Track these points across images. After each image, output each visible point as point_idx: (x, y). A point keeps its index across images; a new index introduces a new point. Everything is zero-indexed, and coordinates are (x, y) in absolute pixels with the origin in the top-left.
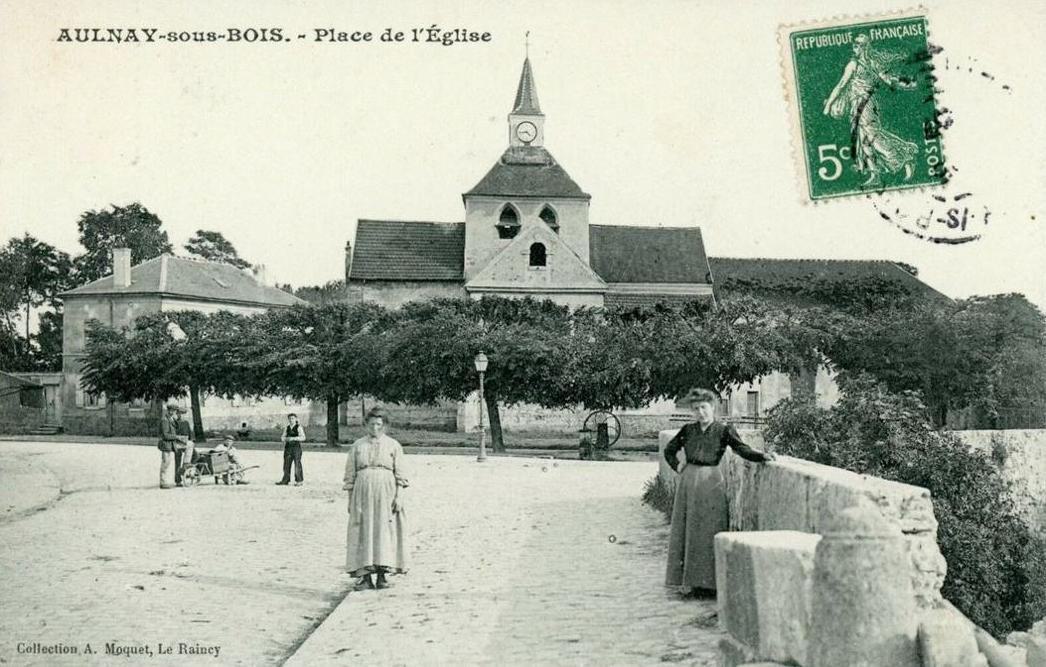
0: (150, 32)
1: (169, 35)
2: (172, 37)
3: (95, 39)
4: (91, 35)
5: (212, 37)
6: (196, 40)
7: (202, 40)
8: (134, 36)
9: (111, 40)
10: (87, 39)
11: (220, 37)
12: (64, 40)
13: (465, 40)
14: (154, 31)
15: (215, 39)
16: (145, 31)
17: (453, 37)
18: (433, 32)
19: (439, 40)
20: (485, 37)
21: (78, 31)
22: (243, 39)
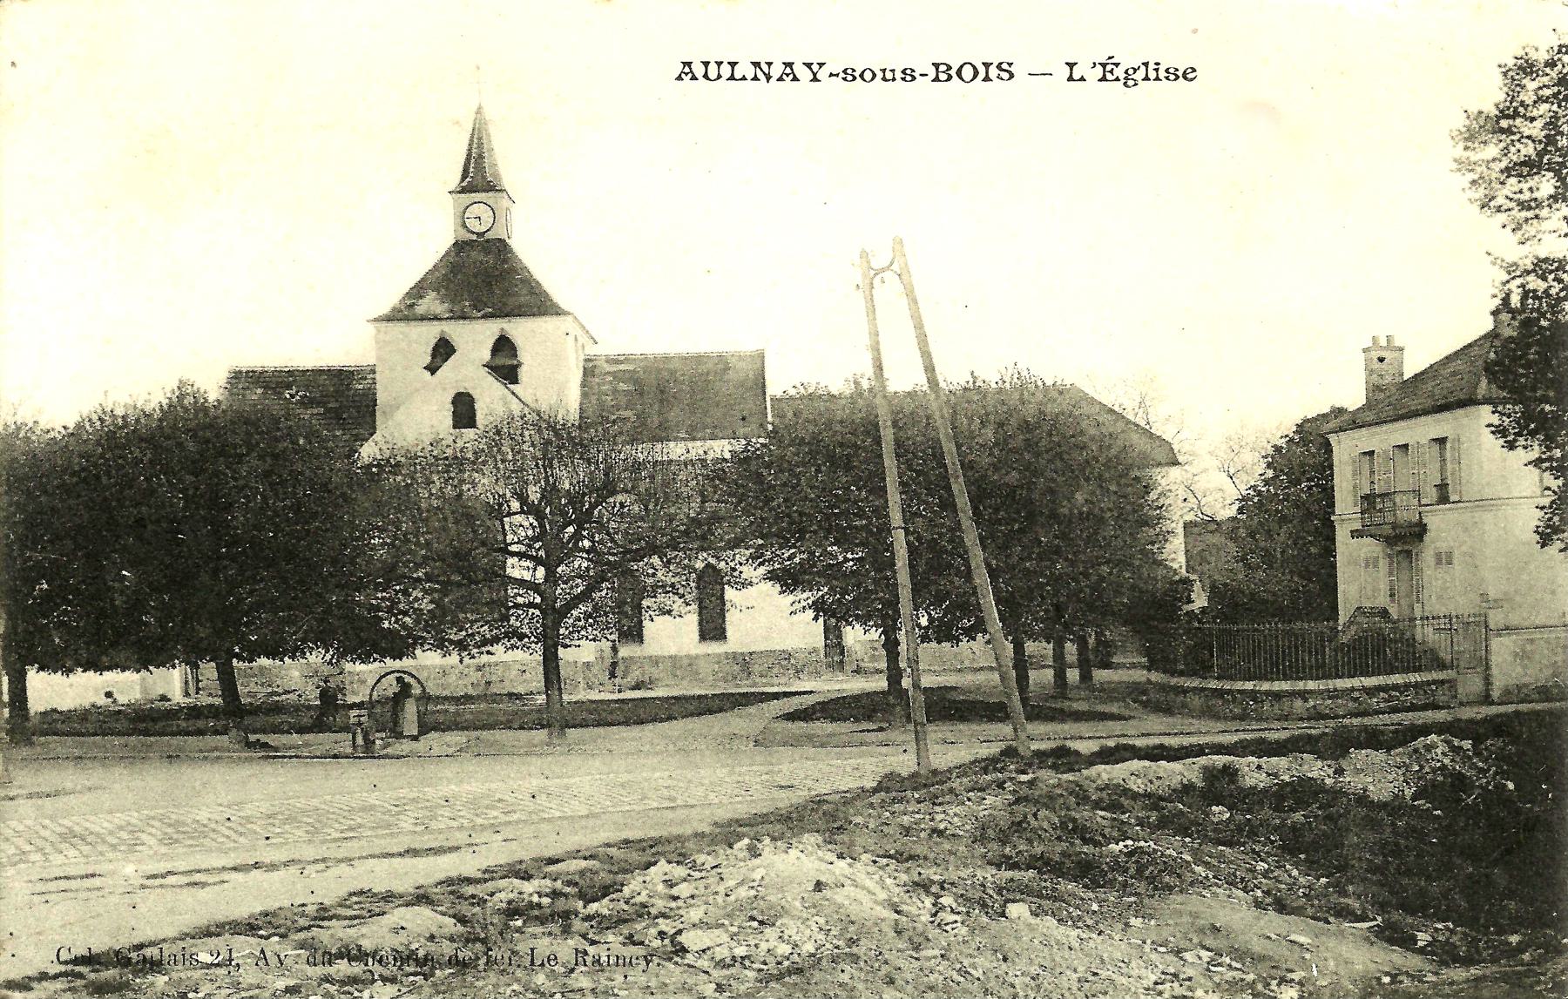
0: (815, 68)
1: (845, 71)
2: (849, 75)
3: (732, 78)
4: (726, 70)
5: (909, 75)
6: (884, 79)
7: (894, 79)
8: (691, 72)
9: (755, 78)
10: (719, 77)
11: (837, 75)
12: (687, 78)
13: (1157, 79)
14: (821, 65)
15: (914, 78)
16: (809, 65)
17: (1141, 74)
18: (1109, 68)
19: (1117, 79)
20: (1188, 75)
21: (706, 64)
22: (859, 78)
